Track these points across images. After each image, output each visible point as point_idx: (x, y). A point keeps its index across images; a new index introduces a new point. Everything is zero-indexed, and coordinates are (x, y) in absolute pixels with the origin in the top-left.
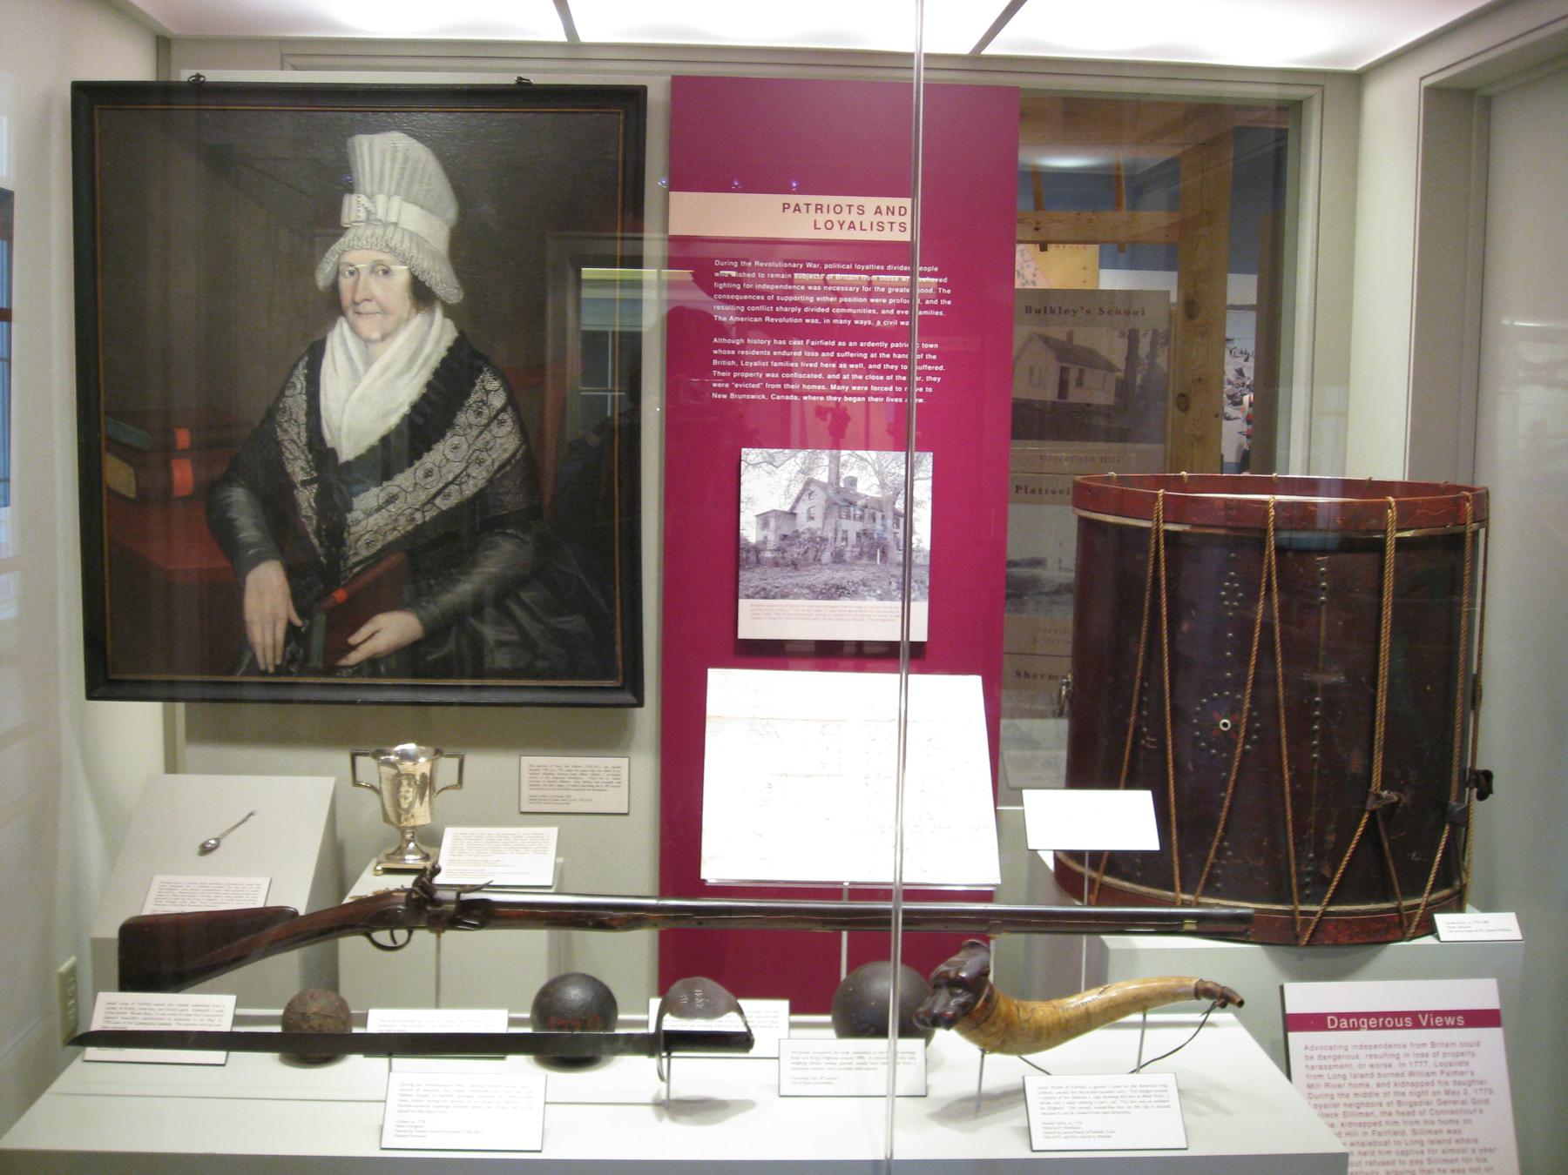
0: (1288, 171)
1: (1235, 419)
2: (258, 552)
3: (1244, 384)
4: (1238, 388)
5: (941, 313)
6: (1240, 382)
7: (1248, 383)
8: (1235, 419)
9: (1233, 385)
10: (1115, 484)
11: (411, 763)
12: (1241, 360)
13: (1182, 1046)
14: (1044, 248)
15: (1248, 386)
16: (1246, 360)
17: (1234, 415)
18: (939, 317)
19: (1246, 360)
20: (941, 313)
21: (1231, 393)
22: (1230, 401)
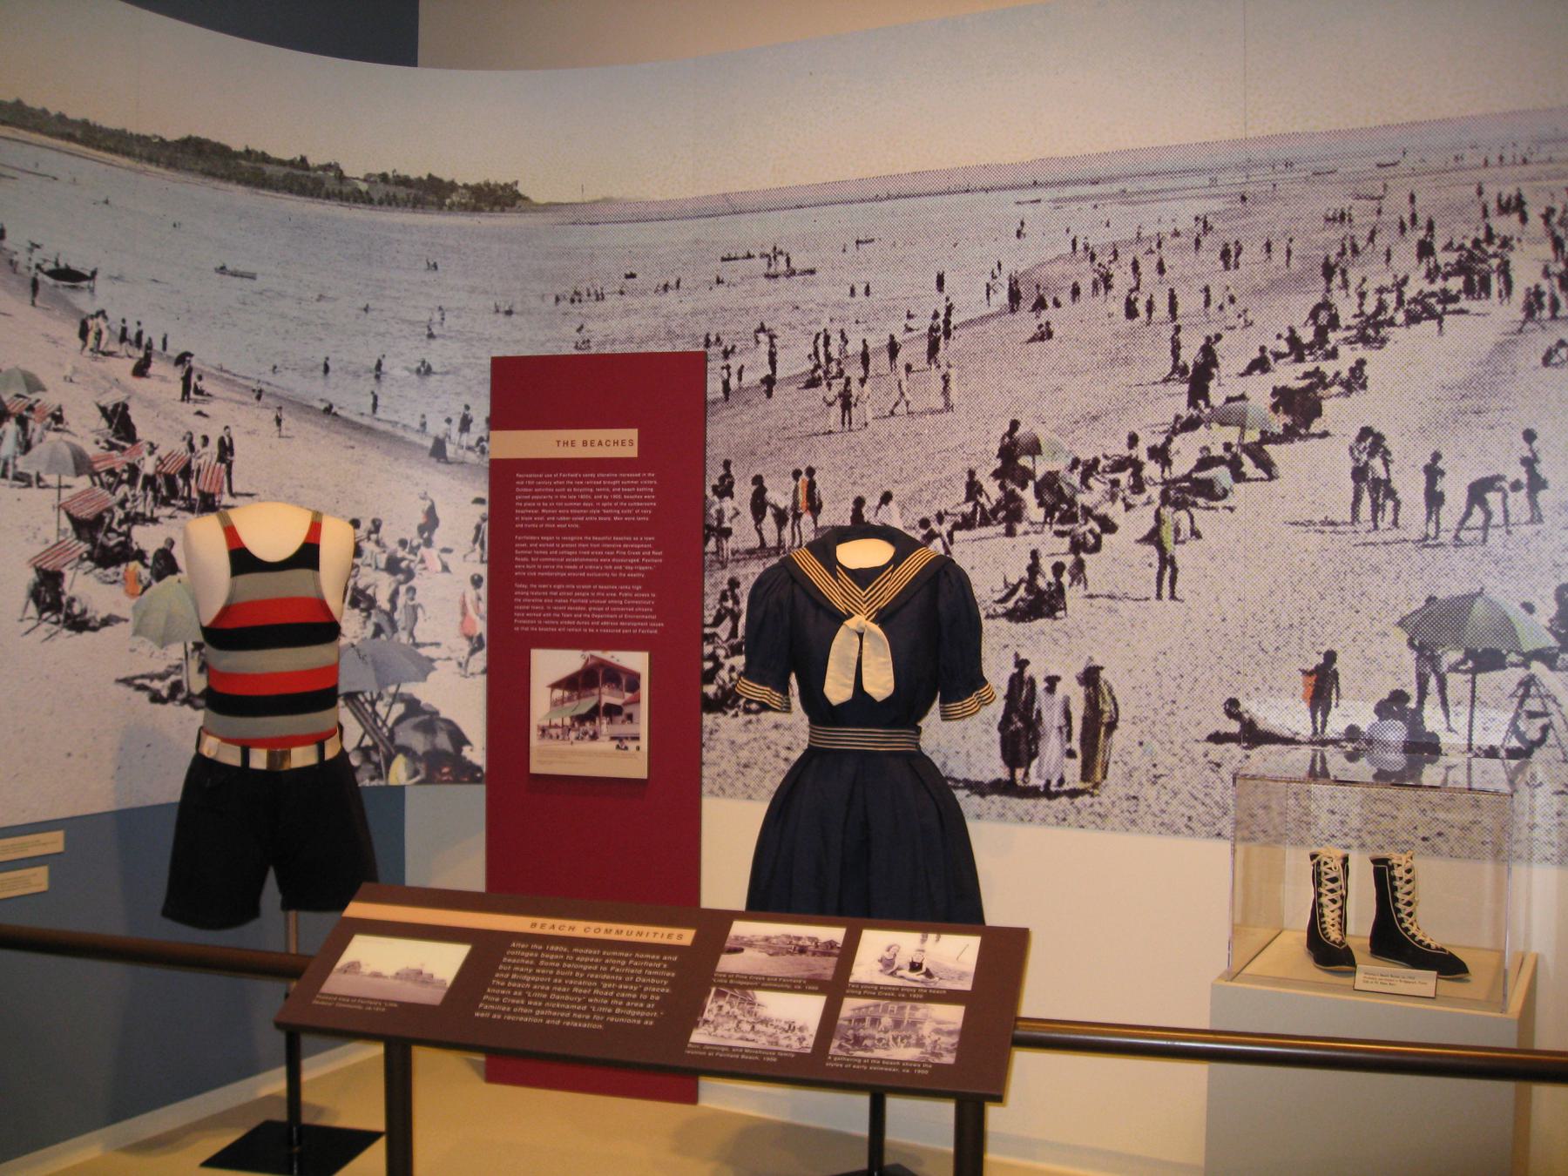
0: (702, 193)
1: (108, 621)
2: (1311, 383)
3: (134, 470)
4: (111, 488)
5: (1034, 717)
6: (119, 461)
7: (148, 466)
8: (108, 621)
9: (94, 474)
10: (910, 1014)
11: (1340, 284)
12: (122, 367)
13: (1519, 972)
14: (303, 160)
15: (150, 481)
16: (141, 370)
17: (99, 610)
18: (798, 677)
19: (141, 370)
20: (1034, 717)
21: (86, 512)
22: (85, 547)
